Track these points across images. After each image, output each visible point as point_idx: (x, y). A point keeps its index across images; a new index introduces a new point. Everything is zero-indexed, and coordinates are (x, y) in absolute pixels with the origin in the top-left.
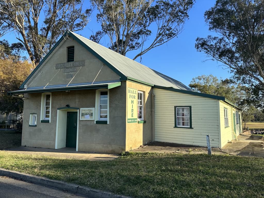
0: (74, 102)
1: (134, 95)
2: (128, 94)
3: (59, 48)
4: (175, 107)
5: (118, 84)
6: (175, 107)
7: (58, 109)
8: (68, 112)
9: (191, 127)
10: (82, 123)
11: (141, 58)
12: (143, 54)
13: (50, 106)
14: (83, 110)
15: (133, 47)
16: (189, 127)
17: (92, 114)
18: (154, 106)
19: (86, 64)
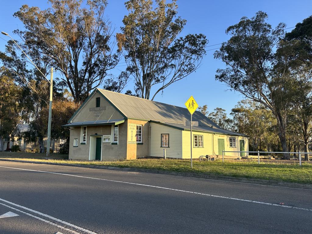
0: (100, 132)
1: (134, 127)
2: (129, 127)
3: (91, 98)
4: (161, 134)
5: (123, 121)
7: (91, 136)
8: (97, 138)
9: (169, 147)
10: (104, 144)
11: (163, 92)
12: (165, 88)
13: (86, 134)
14: (104, 137)
15: (158, 81)
16: (168, 146)
17: (109, 138)
18: (150, 134)
19: (106, 109)
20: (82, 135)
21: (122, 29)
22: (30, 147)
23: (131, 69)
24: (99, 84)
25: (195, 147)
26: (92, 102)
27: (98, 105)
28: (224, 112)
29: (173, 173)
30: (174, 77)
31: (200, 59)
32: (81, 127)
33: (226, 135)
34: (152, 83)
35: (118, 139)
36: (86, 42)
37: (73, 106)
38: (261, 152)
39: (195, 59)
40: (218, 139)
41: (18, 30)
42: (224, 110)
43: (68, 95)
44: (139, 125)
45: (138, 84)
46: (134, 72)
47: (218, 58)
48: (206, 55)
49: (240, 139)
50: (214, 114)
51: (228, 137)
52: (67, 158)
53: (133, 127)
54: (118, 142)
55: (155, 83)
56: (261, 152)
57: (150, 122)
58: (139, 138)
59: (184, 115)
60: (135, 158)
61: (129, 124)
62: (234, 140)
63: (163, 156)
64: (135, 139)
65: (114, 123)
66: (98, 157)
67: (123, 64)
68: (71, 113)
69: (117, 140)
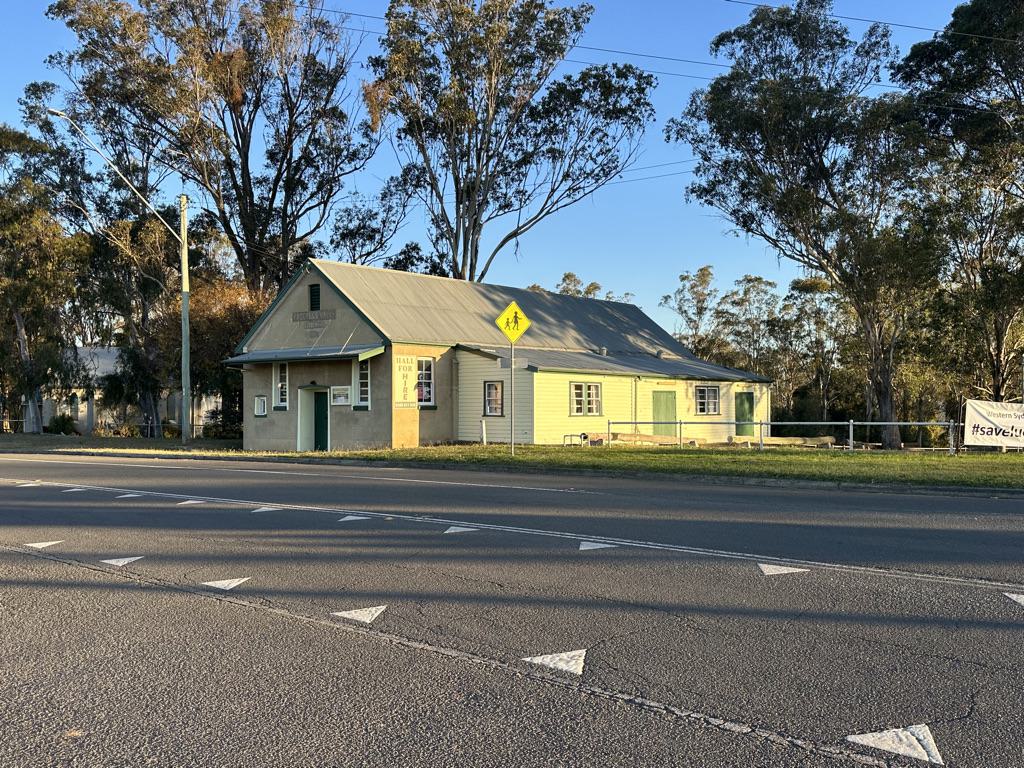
3: (297, 286)
5: (381, 350)
6: (485, 382)
7: (300, 388)
9: (502, 416)
14: (334, 390)
15: (507, 206)
18: (458, 380)
20: (276, 384)
21: (383, 44)
22: (110, 421)
23: (414, 178)
24: (318, 224)
25: (699, 413)
26: (299, 294)
27: (315, 304)
28: (771, 291)
29: (473, 467)
30: (549, 197)
31: (637, 135)
32: (271, 365)
33: (683, 379)
34: (485, 216)
35: (369, 396)
36: (273, 92)
37: (244, 300)
38: (857, 423)
39: (617, 139)
40: (654, 392)
41: (61, 56)
42: (770, 284)
43: (226, 258)
44: (424, 359)
45: (439, 220)
46: (425, 187)
47: (680, 141)
48: (655, 120)
49: (739, 390)
50: (736, 298)
51: (691, 384)
52: (239, 447)
53: (407, 365)
54: (369, 403)
55: (494, 215)
56: (857, 423)
57: (457, 348)
58: (425, 393)
59: (571, 323)
60: (415, 444)
61: (395, 357)
62: (715, 392)
63: (479, 440)
64: (413, 395)
65: (357, 356)
66: (320, 442)
67: (392, 156)
68: (243, 323)
69: (366, 399)
